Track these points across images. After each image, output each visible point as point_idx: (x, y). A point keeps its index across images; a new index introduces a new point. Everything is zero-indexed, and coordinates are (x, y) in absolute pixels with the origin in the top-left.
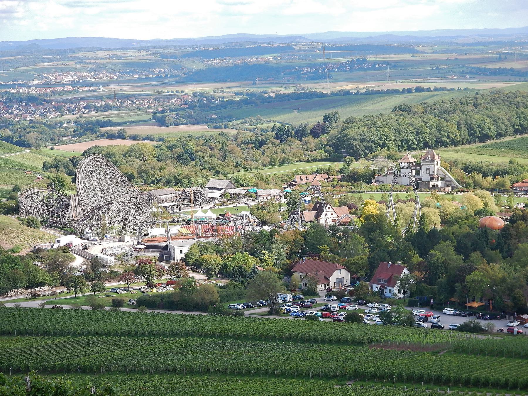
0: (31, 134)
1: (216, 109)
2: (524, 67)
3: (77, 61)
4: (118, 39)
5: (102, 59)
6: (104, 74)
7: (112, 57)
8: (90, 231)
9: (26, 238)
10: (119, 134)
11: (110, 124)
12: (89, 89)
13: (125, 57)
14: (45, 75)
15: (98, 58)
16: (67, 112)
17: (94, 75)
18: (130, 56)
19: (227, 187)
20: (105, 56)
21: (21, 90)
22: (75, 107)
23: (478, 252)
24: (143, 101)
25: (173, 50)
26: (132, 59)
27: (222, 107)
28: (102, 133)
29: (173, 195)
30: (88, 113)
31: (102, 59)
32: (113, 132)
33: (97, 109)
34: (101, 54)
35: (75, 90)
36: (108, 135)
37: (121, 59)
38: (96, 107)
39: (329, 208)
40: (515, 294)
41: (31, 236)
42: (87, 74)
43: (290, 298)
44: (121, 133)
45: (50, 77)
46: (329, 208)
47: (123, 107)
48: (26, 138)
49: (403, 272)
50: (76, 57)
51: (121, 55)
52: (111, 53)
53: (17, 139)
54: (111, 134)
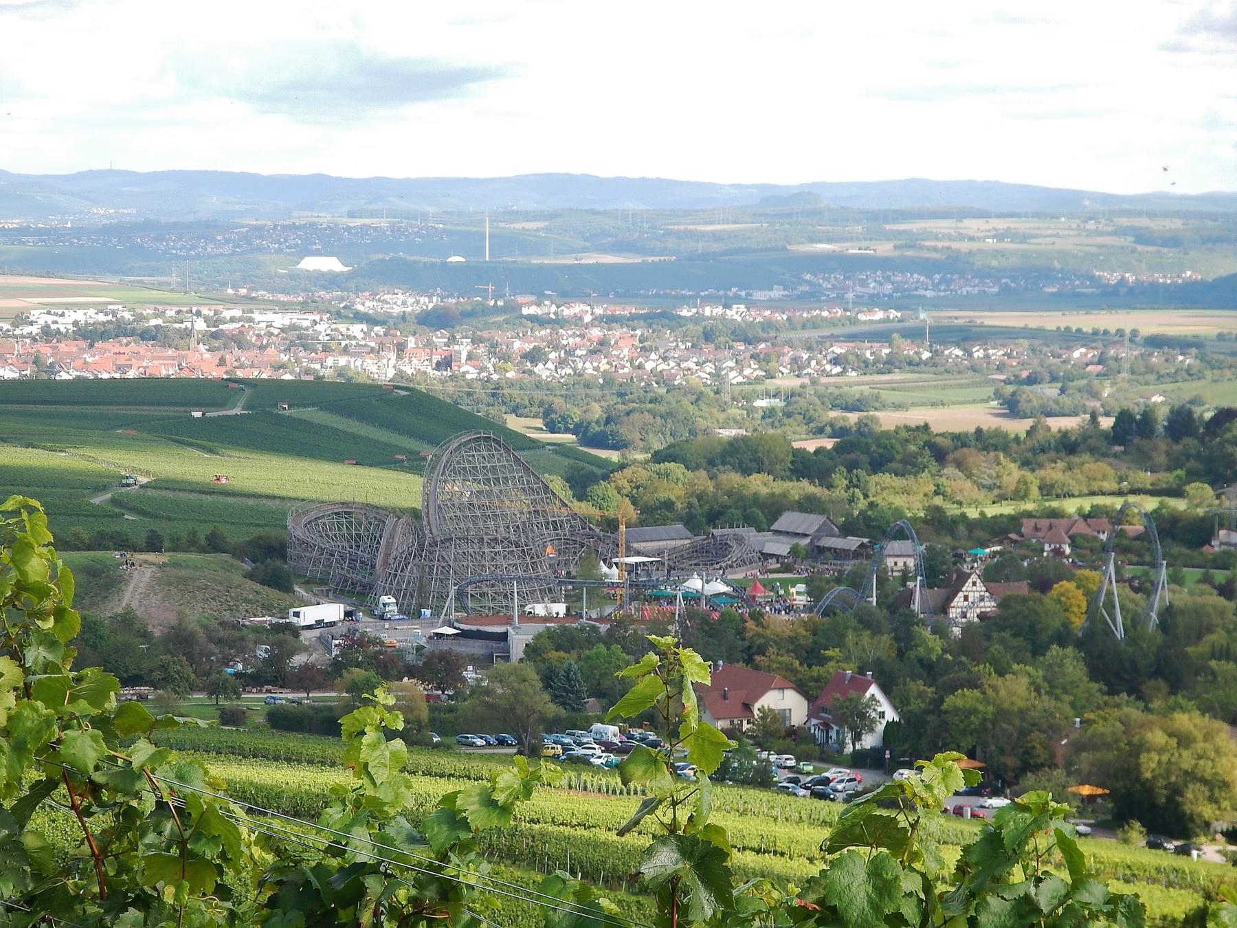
0: (636, 415)
1: (1171, 380)
2: (645, 207)
3: (899, 243)
4: (1049, 189)
5: (971, 239)
6: (967, 280)
7: (1000, 236)
8: (393, 600)
9: (231, 604)
10: (859, 428)
11: (877, 405)
12: (888, 317)
13: (1036, 236)
14: (808, 277)
15: (961, 237)
16: (785, 371)
17: (940, 282)
18: (1051, 236)
19: (818, 530)
20: (986, 231)
21: (707, 311)
22: (810, 359)
23: (1160, 679)
24: (994, 351)
25: (1178, 224)
26: (1053, 244)
27: (1190, 375)
28: (820, 425)
29: (689, 541)
30: (838, 375)
31: (971, 239)
32: (847, 424)
33: (865, 366)
34: (973, 226)
35: (849, 318)
36: (833, 430)
37: (1024, 243)
38: (866, 362)
39: (974, 584)
40: (1027, 742)
41: (247, 601)
42: (922, 278)
43: (615, 735)
44: (866, 425)
45: (821, 281)
46: (974, 584)
47: (935, 365)
48: (619, 426)
49: (868, 695)
50: (904, 232)
51: (1027, 231)
52: (1001, 224)
53: (597, 429)
54: (841, 428)
